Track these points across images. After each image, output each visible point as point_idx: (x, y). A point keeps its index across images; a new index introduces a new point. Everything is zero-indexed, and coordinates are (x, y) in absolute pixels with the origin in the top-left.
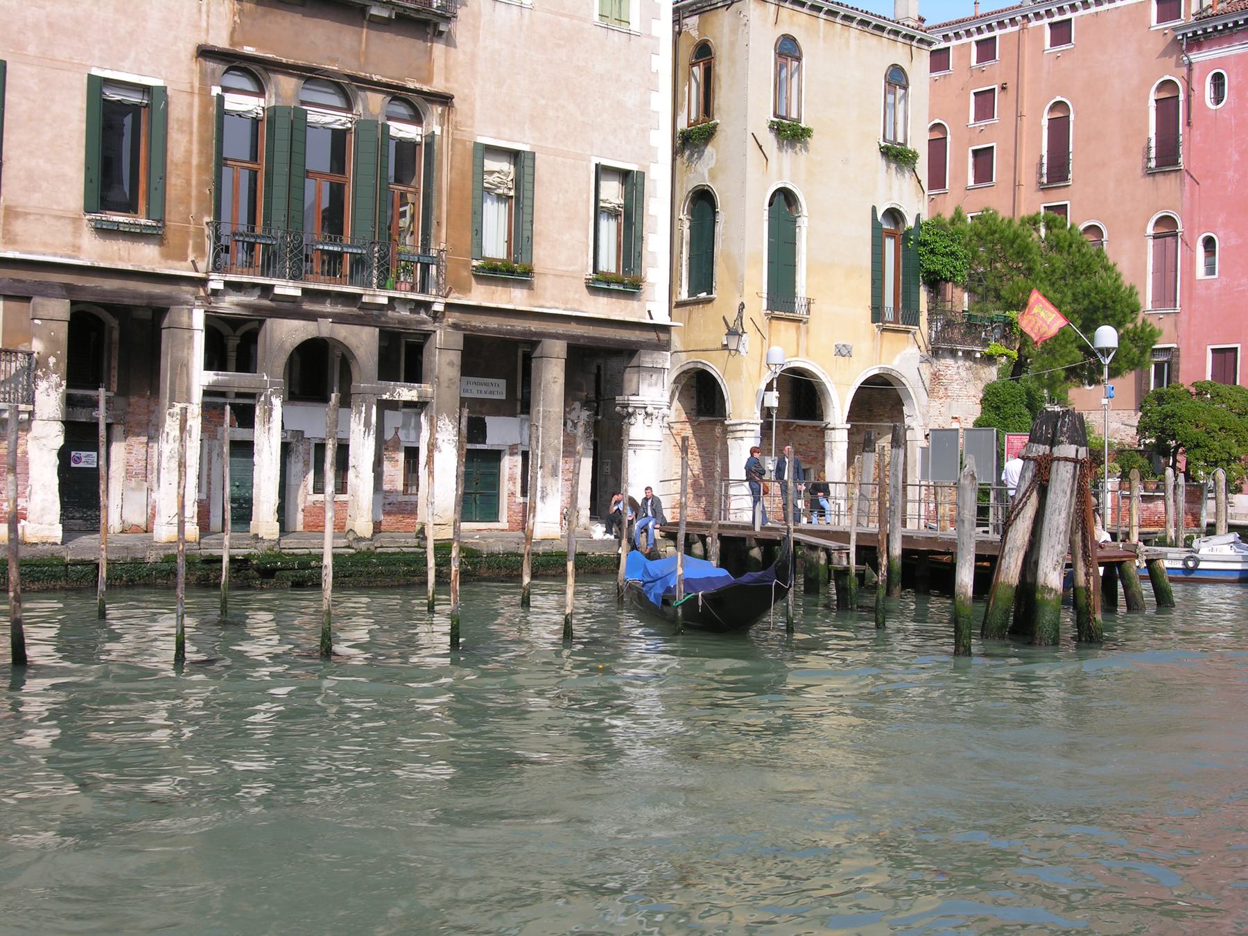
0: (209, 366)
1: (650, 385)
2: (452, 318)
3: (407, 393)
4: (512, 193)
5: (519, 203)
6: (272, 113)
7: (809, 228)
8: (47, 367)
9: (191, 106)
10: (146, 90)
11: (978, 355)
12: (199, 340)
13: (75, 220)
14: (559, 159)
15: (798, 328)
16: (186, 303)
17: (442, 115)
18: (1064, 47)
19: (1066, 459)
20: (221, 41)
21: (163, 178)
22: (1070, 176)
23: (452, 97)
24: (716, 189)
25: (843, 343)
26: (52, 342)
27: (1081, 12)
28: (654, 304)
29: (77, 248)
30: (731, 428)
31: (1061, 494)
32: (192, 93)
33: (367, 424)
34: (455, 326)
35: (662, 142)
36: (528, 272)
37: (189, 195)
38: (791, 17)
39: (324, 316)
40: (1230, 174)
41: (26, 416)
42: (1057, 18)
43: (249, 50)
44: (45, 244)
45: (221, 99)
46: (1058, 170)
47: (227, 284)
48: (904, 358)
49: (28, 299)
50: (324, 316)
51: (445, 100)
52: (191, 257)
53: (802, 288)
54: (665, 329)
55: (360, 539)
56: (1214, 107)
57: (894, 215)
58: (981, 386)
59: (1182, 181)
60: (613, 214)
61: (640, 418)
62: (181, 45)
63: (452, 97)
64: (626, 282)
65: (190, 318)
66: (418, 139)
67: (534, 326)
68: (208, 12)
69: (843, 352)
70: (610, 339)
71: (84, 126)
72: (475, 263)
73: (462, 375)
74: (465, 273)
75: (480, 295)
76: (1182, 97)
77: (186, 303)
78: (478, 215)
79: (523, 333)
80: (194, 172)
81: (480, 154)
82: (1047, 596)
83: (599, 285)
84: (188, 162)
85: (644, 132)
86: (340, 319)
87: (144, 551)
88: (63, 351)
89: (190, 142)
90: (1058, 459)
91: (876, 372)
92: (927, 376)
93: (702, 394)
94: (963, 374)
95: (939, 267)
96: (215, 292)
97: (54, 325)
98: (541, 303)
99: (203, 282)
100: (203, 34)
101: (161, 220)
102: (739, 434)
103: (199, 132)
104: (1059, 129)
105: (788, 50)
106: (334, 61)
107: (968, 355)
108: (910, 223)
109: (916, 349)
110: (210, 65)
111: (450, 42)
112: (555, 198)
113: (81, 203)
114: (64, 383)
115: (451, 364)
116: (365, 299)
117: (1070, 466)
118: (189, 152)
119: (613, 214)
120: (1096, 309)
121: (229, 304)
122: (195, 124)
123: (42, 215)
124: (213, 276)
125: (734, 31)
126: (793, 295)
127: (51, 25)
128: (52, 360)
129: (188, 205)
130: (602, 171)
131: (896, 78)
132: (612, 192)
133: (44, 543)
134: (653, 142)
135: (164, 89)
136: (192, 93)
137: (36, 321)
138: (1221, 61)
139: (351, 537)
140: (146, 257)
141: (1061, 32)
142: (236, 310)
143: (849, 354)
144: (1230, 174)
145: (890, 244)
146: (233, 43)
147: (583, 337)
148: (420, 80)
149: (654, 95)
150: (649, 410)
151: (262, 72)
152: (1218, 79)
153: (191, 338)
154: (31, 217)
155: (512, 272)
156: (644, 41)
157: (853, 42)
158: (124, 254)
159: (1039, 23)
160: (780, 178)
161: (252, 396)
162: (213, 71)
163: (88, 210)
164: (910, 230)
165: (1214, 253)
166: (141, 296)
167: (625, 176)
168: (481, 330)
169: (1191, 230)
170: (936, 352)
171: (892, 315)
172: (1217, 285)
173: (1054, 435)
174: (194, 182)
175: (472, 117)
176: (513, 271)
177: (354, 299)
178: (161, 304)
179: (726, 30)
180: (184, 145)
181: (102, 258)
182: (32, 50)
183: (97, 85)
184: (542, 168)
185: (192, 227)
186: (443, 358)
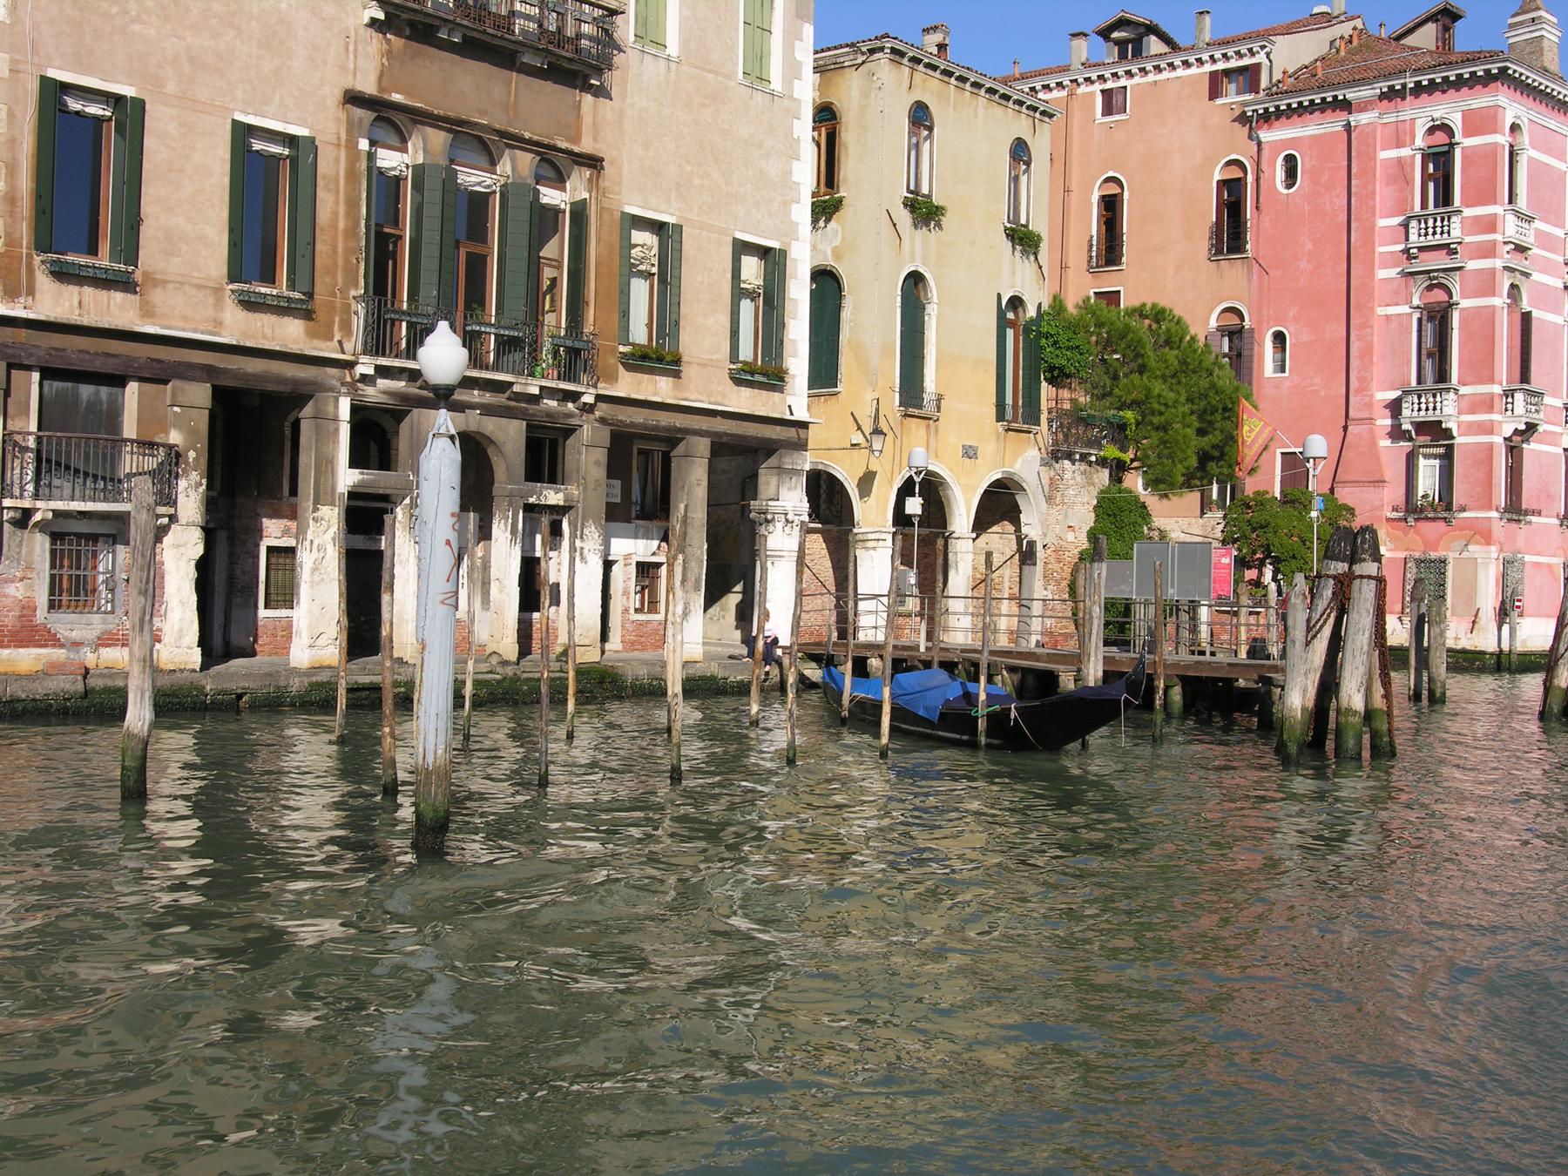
0: (353, 464)
1: (790, 489)
2: (602, 410)
3: (553, 497)
4: (654, 270)
5: (666, 279)
6: (419, 171)
7: (938, 316)
8: (187, 463)
9: (337, 160)
10: (291, 140)
11: (1093, 458)
12: (345, 432)
13: (218, 291)
14: (704, 233)
15: (928, 427)
16: (332, 389)
17: (590, 180)
18: (1117, 117)
19: (1370, 577)
20: (369, 87)
21: (313, 243)
22: (1124, 259)
23: (602, 160)
24: (842, 271)
25: (969, 445)
26: (191, 433)
27: (1137, 80)
28: (796, 400)
29: (219, 323)
30: (860, 537)
31: (1364, 614)
32: (339, 145)
33: (514, 532)
34: (602, 420)
35: (802, 212)
36: (677, 361)
37: (335, 263)
38: (924, 81)
39: (473, 406)
40: (1303, 264)
41: (165, 520)
42: (1109, 85)
43: (397, 97)
44: (185, 318)
45: (371, 157)
46: (1110, 250)
47: (378, 368)
48: (1025, 460)
49: (166, 382)
50: (473, 406)
51: (593, 162)
52: (337, 337)
53: (930, 384)
54: (804, 425)
55: (505, 663)
56: (1286, 191)
57: (1016, 302)
58: (1095, 492)
59: (1250, 270)
60: (752, 295)
61: (779, 525)
62: (327, 88)
63: (602, 160)
64: (770, 376)
65: (336, 407)
66: (563, 206)
67: (679, 420)
68: (356, 51)
69: (970, 453)
70: (752, 438)
71: (227, 180)
72: (622, 349)
73: (609, 477)
74: (612, 360)
75: (628, 385)
76: (1250, 178)
77: (332, 389)
78: (625, 293)
79: (669, 429)
80: (340, 237)
81: (627, 226)
82: (1351, 719)
83: (744, 376)
84: (334, 226)
85: (786, 205)
86: (488, 410)
87: (287, 679)
88: (203, 444)
89: (337, 202)
90: (1362, 577)
91: (999, 476)
92: (1046, 481)
93: (829, 503)
94: (1078, 478)
95: (1064, 362)
96: (364, 378)
97: (194, 413)
98: (686, 395)
99: (350, 365)
100: (350, 77)
101: (310, 295)
102: (870, 544)
103: (346, 191)
104: (1111, 206)
105: (920, 117)
106: (483, 114)
107: (1084, 457)
108: (1031, 312)
109: (1036, 451)
110: (359, 112)
111: (602, 92)
112: (699, 278)
113: (224, 270)
114: (204, 481)
115: (597, 463)
116: (516, 388)
117: (1373, 583)
118: (336, 213)
119: (752, 295)
120: (1214, 411)
121: (374, 394)
122: (342, 182)
123: (182, 283)
124: (364, 359)
125: (865, 94)
126: (922, 390)
127: (191, 60)
128: (192, 454)
129: (334, 276)
130: (742, 248)
131: (1020, 152)
132: (752, 270)
133: (182, 671)
134: (794, 218)
135: (312, 140)
136: (339, 145)
137: (176, 409)
138: (1292, 142)
139: (494, 660)
140: (289, 333)
141: (1112, 102)
142: (382, 399)
143: (975, 456)
144: (1303, 264)
145: (1010, 333)
146: (381, 89)
147: (726, 434)
148: (569, 140)
149: (796, 164)
150: (790, 517)
151: (408, 123)
152: (1290, 161)
153: (337, 430)
154: (171, 286)
155: (660, 360)
156: (786, 102)
157: (981, 112)
158: (268, 331)
159: (1090, 88)
160: (913, 260)
161: (385, 498)
162: (361, 120)
163: (232, 279)
164: (1031, 320)
165: (1284, 350)
166: (285, 381)
167: (764, 252)
168: (627, 426)
169: (1259, 323)
170: (1056, 455)
171: (1016, 412)
172: (1287, 384)
173: (1354, 552)
174: (340, 250)
175: (620, 183)
176: (660, 358)
177: (501, 387)
178: (306, 390)
179: (855, 92)
180: (337, 211)
181: (245, 335)
182: (171, 88)
183: (242, 133)
184: (689, 244)
185: (338, 302)
186: (587, 454)
